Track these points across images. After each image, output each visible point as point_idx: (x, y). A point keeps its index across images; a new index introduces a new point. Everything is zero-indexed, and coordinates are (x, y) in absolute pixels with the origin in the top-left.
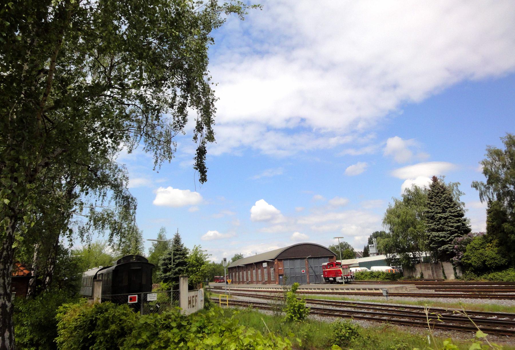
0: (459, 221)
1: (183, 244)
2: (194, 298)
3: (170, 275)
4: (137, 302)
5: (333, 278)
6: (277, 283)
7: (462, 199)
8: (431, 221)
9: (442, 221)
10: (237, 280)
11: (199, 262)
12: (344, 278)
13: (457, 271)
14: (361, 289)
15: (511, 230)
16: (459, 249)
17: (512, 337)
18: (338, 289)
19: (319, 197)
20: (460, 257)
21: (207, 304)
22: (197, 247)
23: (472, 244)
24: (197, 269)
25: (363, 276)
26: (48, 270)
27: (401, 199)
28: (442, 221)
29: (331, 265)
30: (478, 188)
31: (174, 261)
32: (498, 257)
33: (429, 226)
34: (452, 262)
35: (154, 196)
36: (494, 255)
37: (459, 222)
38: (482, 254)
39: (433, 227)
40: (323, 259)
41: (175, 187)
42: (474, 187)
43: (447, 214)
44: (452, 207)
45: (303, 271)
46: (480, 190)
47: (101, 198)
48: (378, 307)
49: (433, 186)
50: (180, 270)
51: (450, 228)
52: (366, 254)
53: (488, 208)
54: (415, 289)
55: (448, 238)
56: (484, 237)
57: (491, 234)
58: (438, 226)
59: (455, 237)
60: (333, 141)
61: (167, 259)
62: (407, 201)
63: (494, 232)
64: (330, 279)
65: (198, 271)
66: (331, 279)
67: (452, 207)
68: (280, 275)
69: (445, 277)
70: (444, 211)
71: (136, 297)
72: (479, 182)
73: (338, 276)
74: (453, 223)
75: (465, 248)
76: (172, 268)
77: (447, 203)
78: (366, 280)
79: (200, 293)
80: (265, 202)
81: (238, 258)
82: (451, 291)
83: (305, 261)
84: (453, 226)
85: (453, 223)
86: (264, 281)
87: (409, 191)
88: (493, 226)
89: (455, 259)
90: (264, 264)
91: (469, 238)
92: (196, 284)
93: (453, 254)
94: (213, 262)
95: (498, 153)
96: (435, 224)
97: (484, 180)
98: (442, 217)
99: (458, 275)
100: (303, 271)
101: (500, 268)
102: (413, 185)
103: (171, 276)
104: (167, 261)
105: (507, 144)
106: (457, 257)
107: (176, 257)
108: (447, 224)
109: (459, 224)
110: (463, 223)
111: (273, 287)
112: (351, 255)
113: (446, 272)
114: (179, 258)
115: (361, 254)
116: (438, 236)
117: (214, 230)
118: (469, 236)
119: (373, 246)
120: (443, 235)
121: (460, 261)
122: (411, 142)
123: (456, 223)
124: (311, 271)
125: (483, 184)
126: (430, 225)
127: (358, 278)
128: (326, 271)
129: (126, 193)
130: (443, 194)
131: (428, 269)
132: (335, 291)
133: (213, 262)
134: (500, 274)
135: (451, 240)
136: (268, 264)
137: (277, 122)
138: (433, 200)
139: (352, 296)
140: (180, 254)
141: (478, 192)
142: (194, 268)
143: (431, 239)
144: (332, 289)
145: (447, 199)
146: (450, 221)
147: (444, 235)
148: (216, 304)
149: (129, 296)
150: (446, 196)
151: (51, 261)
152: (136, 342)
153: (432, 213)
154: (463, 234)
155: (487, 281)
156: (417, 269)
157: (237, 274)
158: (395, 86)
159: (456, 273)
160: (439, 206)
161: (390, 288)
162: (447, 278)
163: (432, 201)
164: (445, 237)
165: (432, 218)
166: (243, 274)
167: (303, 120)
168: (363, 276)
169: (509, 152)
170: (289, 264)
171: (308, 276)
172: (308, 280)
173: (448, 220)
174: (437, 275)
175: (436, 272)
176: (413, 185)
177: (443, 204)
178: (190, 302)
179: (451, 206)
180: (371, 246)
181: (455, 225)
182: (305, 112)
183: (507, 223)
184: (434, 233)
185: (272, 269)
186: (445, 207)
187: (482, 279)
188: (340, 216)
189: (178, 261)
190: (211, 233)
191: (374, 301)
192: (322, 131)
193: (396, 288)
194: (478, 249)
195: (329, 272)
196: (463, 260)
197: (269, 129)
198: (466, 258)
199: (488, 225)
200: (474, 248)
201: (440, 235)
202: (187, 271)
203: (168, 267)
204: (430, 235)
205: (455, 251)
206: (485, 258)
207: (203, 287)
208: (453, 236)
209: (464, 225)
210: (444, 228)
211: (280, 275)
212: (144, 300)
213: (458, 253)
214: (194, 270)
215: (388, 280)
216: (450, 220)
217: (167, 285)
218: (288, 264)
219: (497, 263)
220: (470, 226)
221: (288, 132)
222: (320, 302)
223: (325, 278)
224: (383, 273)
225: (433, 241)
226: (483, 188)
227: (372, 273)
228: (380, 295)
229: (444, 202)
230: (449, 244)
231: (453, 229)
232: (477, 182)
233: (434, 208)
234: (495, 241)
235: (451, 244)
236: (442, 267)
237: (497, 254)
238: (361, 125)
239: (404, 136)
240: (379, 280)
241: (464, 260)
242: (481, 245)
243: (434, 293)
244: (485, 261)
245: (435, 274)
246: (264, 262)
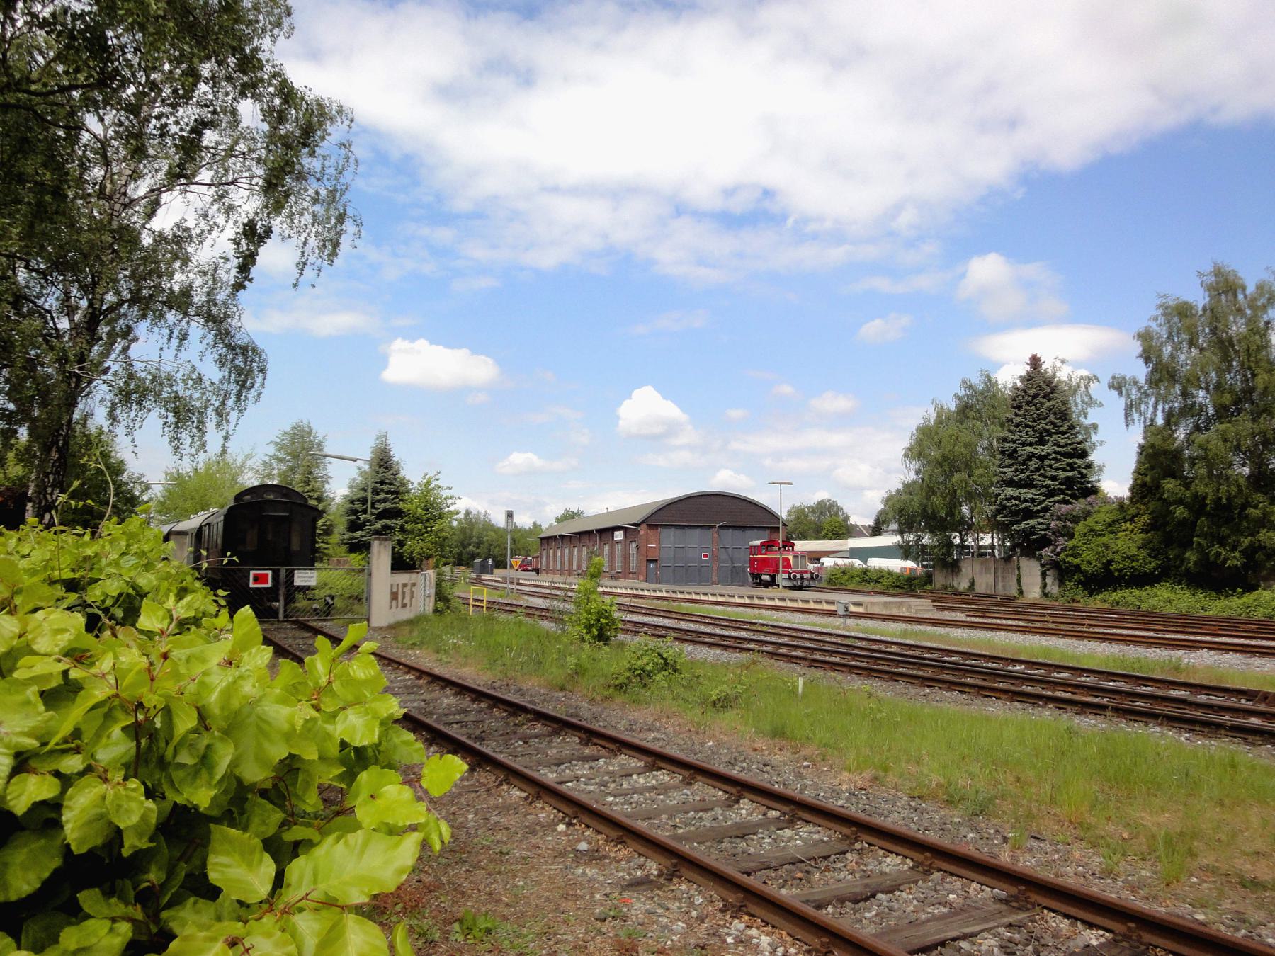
0: (1072, 467)
2: (407, 590)
3: (362, 536)
4: (269, 585)
6: (641, 578)
7: (1093, 416)
8: (1008, 461)
9: (1033, 464)
10: (558, 567)
11: (431, 511)
12: (795, 576)
13: (1049, 580)
14: (812, 603)
15: (1179, 496)
16: (1059, 531)
17: (999, 701)
19: (787, 389)
20: (1058, 549)
21: (441, 605)
22: (430, 478)
23: (1090, 521)
24: (426, 527)
25: (846, 578)
26: (46, 499)
27: (952, 406)
28: (1033, 464)
29: (769, 545)
30: (1124, 392)
31: (373, 507)
32: (1142, 555)
33: (1001, 473)
34: (1040, 558)
35: (383, 362)
36: (1134, 551)
37: (1072, 469)
38: (1106, 547)
39: (1009, 475)
40: (755, 531)
41: (434, 341)
42: (1114, 388)
43: (1048, 448)
44: (1064, 433)
45: (706, 556)
46: (1128, 396)
47: (175, 342)
48: (806, 636)
49: (1028, 379)
50: (386, 527)
51: (1048, 482)
52: (877, 530)
54: (928, 611)
55: (1041, 503)
56: (1121, 506)
57: (1137, 502)
59: (1056, 502)
60: (837, 254)
61: (358, 500)
62: (965, 410)
63: (1143, 497)
65: (427, 532)
66: (766, 578)
67: (1064, 433)
68: (649, 561)
69: (1021, 593)
70: (1042, 442)
71: (267, 575)
72: (1127, 378)
74: (1057, 469)
75: (1073, 528)
76: (369, 521)
77: (1052, 423)
78: (849, 587)
79: (425, 581)
80: (656, 392)
81: (569, 516)
82: (1000, 618)
83: (713, 533)
84: (1055, 476)
85: (1057, 469)
86: (613, 573)
87: (971, 387)
88: (1144, 485)
89: (1047, 552)
90: (616, 533)
91: (1089, 508)
92: (421, 561)
93: (1045, 542)
94: (468, 513)
95: (1183, 311)
96: (1016, 470)
97: (1141, 372)
98: (1034, 454)
99: (1048, 588)
100: (706, 556)
101: (1141, 580)
104: (357, 506)
105: (1210, 288)
106: (1051, 548)
107: (378, 497)
108: (1042, 471)
109: (1071, 474)
110: (1080, 473)
112: (842, 530)
113: (1023, 580)
114: (385, 501)
115: (867, 530)
117: (526, 452)
118: (1090, 504)
121: (1058, 559)
122: (1032, 270)
123: (1064, 470)
124: (723, 556)
125: (1135, 383)
126: (1004, 470)
127: (839, 581)
129: (240, 339)
130: (1049, 400)
131: (987, 571)
132: (757, 602)
133: (468, 513)
134: (1137, 592)
135: (1046, 509)
136: (625, 535)
137: (703, 193)
138: (1021, 413)
139: (769, 612)
140: (387, 493)
141: (1121, 403)
142: (420, 526)
143: (1001, 503)
144: (751, 597)
145: (1055, 414)
146: (1050, 466)
147: (1032, 496)
148: (462, 607)
149: (252, 573)
150: (1053, 406)
151: (54, 479)
153: (1014, 442)
154: (1076, 498)
155: (1106, 606)
156: (964, 570)
157: (559, 554)
158: (1013, 123)
159: (1045, 586)
162: (1025, 594)
163: (1019, 415)
164: (1032, 501)
165: (1012, 454)
166: (571, 553)
167: (768, 193)
168: (846, 578)
169: (1212, 310)
170: (672, 538)
171: (715, 568)
172: (714, 578)
173: (1047, 462)
174: (1004, 587)
177: (1043, 425)
178: (394, 596)
179: (1061, 429)
181: (1062, 474)
182: (775, 173)
183: (1172, 481)
185: (634, 546)
186: (1047, 431)
187: (1098, 602)
188: (837, 439)
189: (381, 507)
190: (519, 459)
191: (815, 625)
192: (812, 227)
194: (1100, 535)
196: (1063, 556)
197: (680, 209)
198: (1070, 552)
199: (1135, 480)
200: (1092, 530)
201: (1023, 496)
202: (403, 529)
203: (359, 519)
204: (999, 495)
205: (1049, 533)
206: (1111, 557)
207: (436, 567)
208: (1052, 499)
209: (1083, 476)
210: (1034, 480)
211: (649, 561)
212: (286, 582)
213: (1056, 541)
214: (420, 530)
215: (899, 591)
216: (1053, 462)
217: (363, 559)
218: (670, 538)
220: (1099, 480)
221: (729, 221)
222: (702, 620)
223: (752, 574)
224: (890, 573)
225: (1004, 507)
226: (1134, 394)
227: (865, 572)
228: (831, 614)
229: (1045, 419)
231: (1055, 485)
232: (1124, 378)
233: (1020, 431)
234: (1143, 520)
236: (1019, 568)
237: (1139, 548)
238: (907, 218)
239: (1014, 252)
240: (879, 588)
241: (1067, 556)
242: (1110, 525)
243: (964, 619)
244: (1110, 562)
245: (1000, 584)
246: (618, 528)
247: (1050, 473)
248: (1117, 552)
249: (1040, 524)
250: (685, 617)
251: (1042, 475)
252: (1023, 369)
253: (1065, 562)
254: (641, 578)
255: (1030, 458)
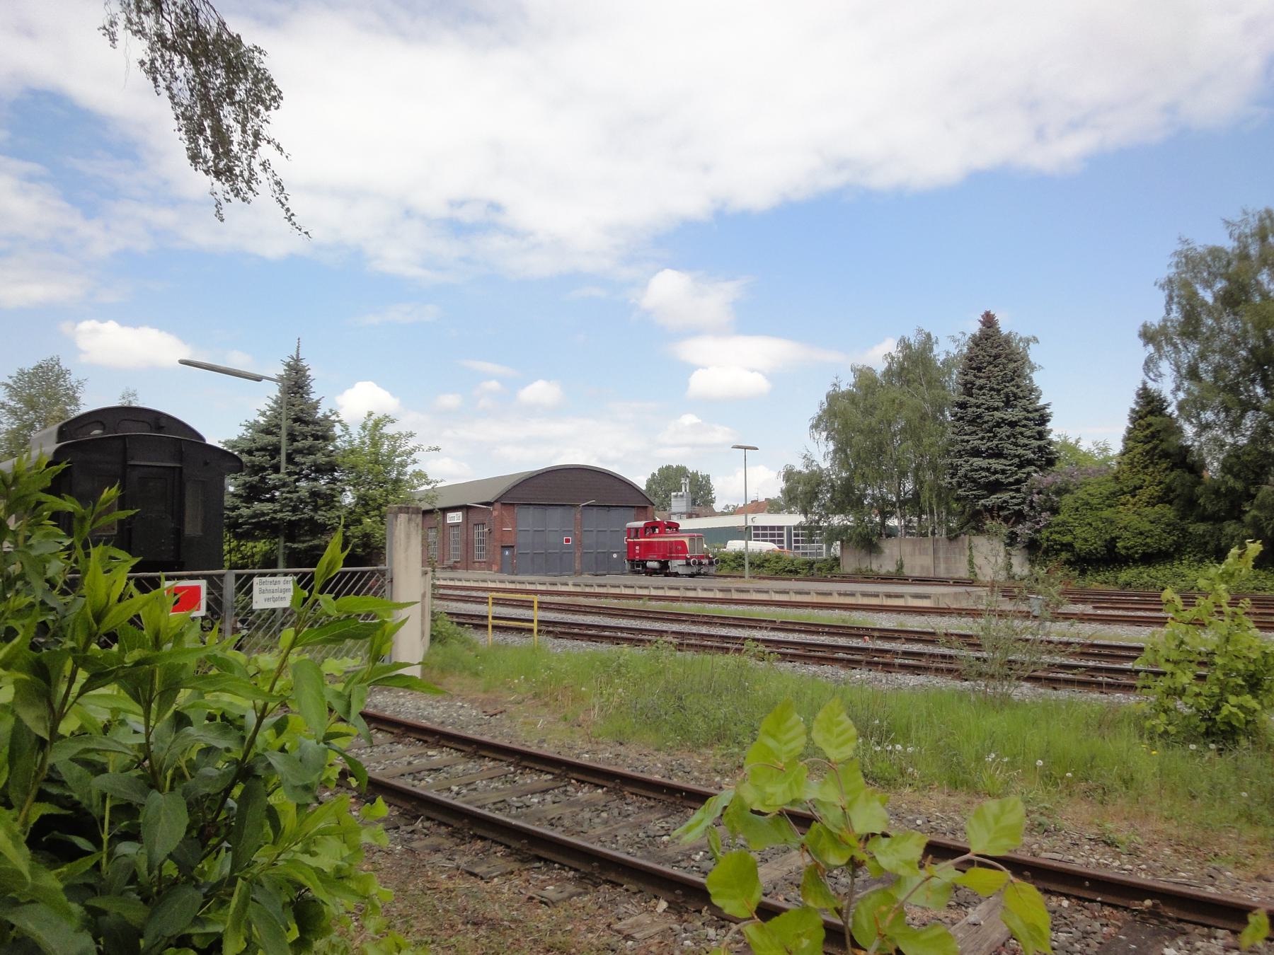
1: (318, 402)
3: (275, 512)
5: (659, 562)
14: (835, 595)
18: (830, 594)
28: (1005, 431)
31: (290, 459)
33: (963, 441)
45: (567, 540)
49: (977, 342)
53: (1134, 406)
55: (1013, 474)
58: (989, 444)
64: (650, 564)
66: (653, 564)
71: (198, 588)
73: (678, 558)
74: (1029, 437)
83: (577, 513)
85: (1029, 437)
87: (908, 347)
90: (450, 515)
96: (982, 439)
98: (1004, 420)
102: (920, 331)
103: (279, 515)
111: (484, 577)
116: (988, 470)
119: (682, 496)
120: (1000, 467)
126: (966, 438)
128: (639, 544)
136: (466, 518)
146: (1021, 434)
152: (232, 798)
153: (978, 407)
156: (887, 551)
160: (998, 391)
161: (943, 595)
164: (1003, 472)
167: (495, 207)
172: (577, 566)
173: (1018, 429)
175: (947, 560)
176: (920, 331)
180: (676, 496)
184: (975, 459)
186: (1015, 395)
193: (956, 595)
195: (649, 547)
197: (409, 213)
200: (1088, 504)
201: (994, 466)
218: (527, 520)
219: (1149, 547)
230: (1012, 490)
235: (1018, 491)
244: (1114, 540)
245: (942, 566)
247: (1022, 441)
248: (1125, 528)
249: (1013, 498)
250: (677, 618)
251: (1013, 444)
252: (975, 327)
253: (1048, 540)
254: (495, 568)
255: (998, 425)
